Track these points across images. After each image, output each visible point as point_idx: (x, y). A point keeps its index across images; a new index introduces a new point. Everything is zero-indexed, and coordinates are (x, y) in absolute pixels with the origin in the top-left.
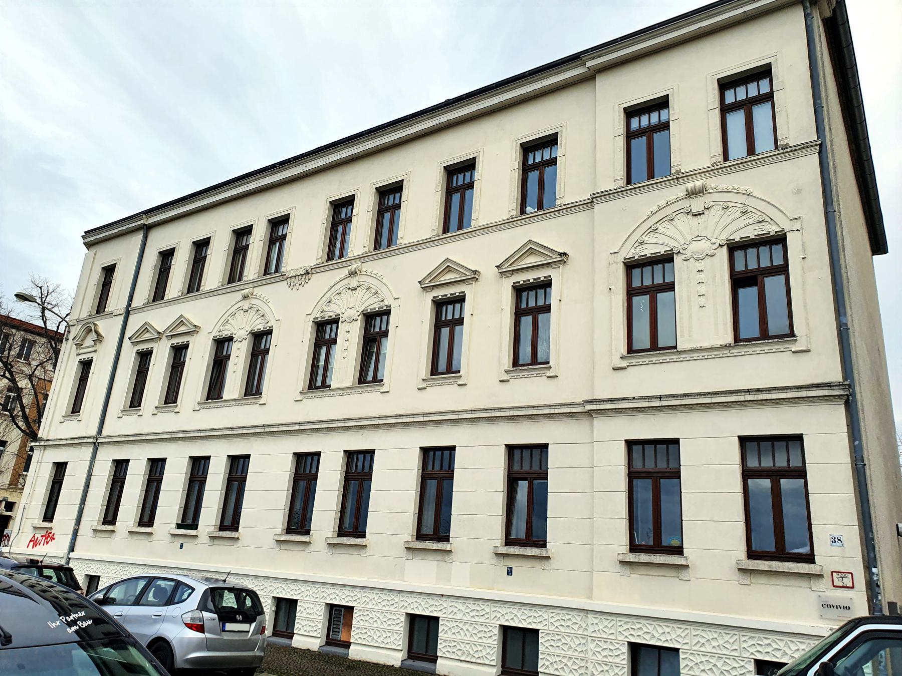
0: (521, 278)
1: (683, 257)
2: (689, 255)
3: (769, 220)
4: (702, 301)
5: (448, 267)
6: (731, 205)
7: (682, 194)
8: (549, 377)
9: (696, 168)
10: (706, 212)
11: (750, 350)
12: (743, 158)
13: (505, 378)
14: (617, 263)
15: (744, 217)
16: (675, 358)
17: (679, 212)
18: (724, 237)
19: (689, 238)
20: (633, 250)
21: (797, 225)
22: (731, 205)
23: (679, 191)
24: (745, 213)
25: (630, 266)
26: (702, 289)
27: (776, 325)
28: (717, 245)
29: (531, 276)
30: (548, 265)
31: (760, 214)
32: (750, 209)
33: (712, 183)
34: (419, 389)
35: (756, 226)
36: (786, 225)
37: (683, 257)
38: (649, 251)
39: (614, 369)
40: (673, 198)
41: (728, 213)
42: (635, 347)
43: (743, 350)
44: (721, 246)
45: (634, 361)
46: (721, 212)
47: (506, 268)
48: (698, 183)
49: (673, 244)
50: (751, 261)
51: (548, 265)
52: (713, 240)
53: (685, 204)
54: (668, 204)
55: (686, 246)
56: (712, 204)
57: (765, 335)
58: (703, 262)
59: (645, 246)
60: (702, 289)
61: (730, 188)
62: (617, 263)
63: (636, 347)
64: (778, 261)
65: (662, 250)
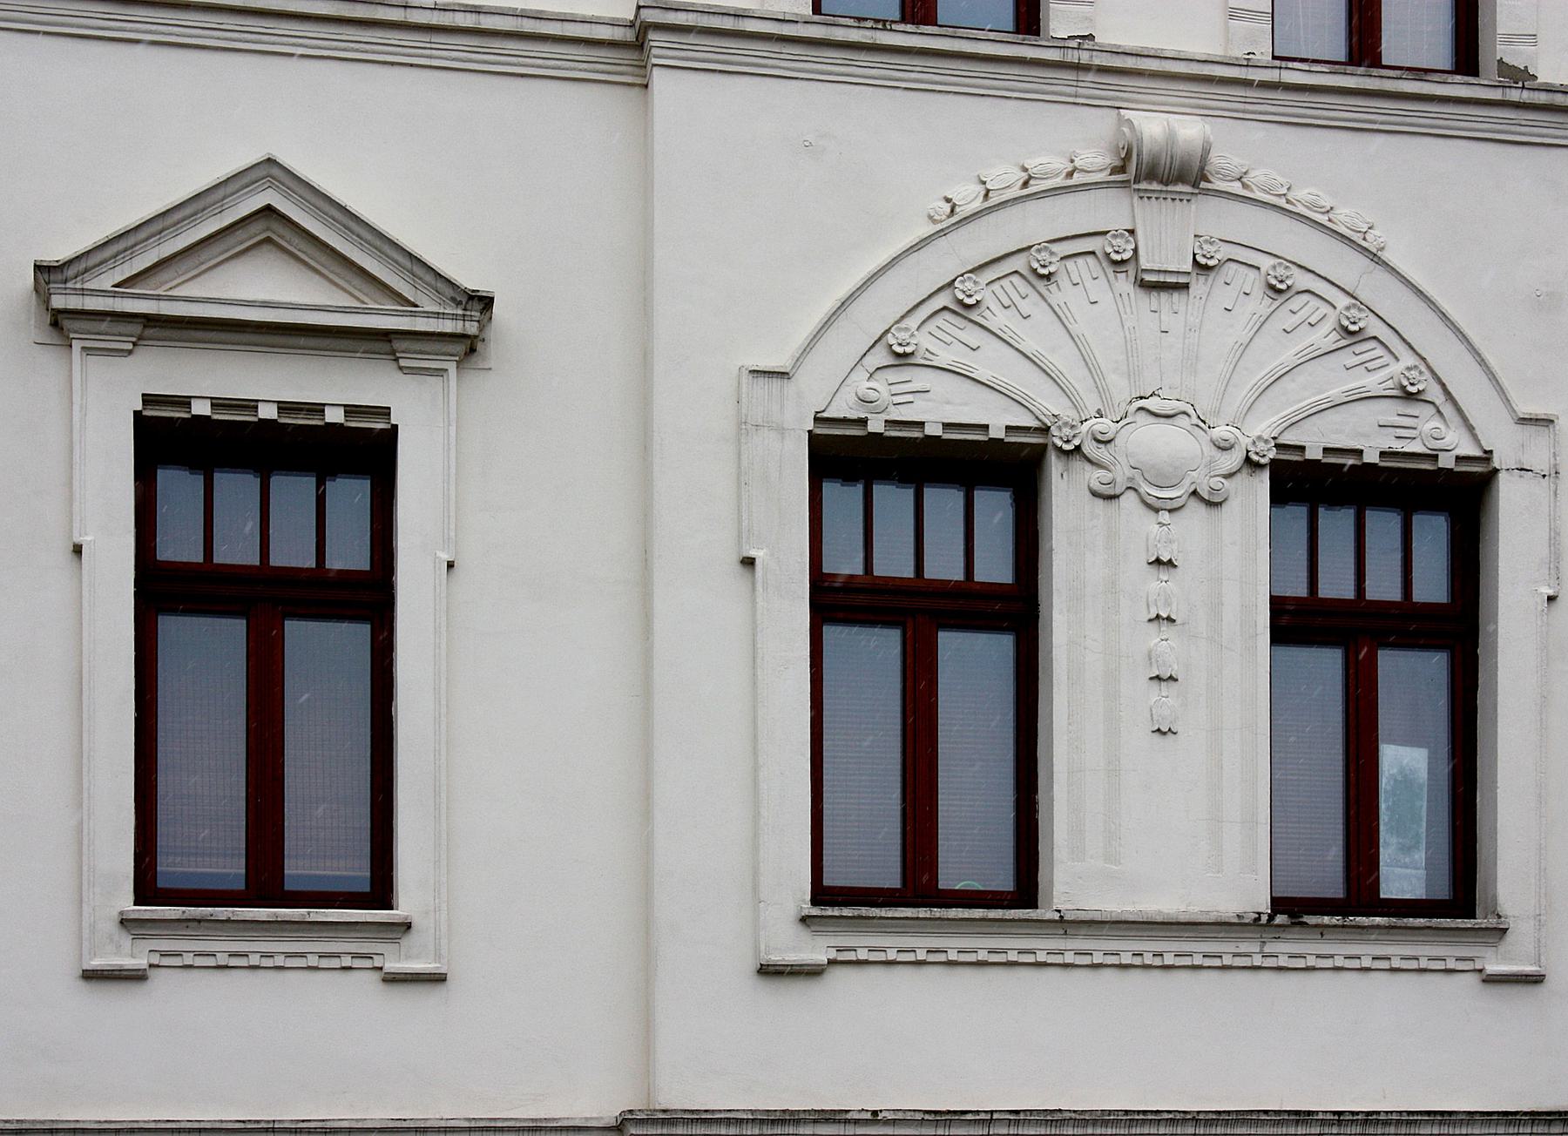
0: (206, 381)
1: (1095, 477)
2: (1121, 474)
3: (1439, 398)
4: (1165, 701)
5: (269, 214)
6: (1302, 280)
7: (1096, 159)
8: (393, 979)
9: (1170, 45)
10: (1199, 286)
11: (1397, 951)
12: (1420, 73)
13: (128, 962)
14: (781, 430)
15: (1348, 358)
16: (1043, 946)
17: (1081, 244)
18: (1261, 430)
19: (1121, 390)
20: (861, 383)
21: (1537, 450)
22: (1302, 280)
23: (1075, 136)
24: (1351, 335)
25: (846, 458)
26: (1168, 648)
27: (319, 842)
28: (1234, 460)
29: (268, 385)
30: (380, 343)
31: (1408, 359)
32: (1375, 328)
33: (1241, 146)
34: (769, 971)
35: (1390, 412)
36: (1506, 445)
37: (1095, 477)
38: (935, 407)
39: (90, 976)
40: (1049, 164)
41: (1284, 319)
42: (1004, 881)
43: (1310, 948)
44: (1250, 464)
45: (862, 944)
46: (1260, 304)
47: (99, 292)
48: (1164, 125)
49: (1050, 404)
50: (242, 523)
51: (380, 343)
52: (1222, 432)
53: (1110, 211)
54: (1030, 191)
55: (1104, 425)
56: (1225, 252)
57: (265, 882)
58: (1178, 524)
59: (921, 379)
60: (1168, 648)
61: (1302, 194)
62: (781, 430)
63: (170, 868)
64: (349, 552)
65: (998, 419)
